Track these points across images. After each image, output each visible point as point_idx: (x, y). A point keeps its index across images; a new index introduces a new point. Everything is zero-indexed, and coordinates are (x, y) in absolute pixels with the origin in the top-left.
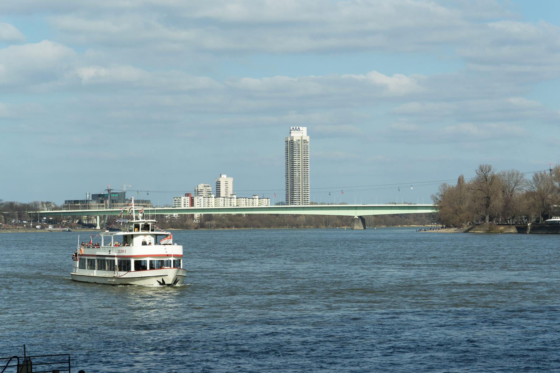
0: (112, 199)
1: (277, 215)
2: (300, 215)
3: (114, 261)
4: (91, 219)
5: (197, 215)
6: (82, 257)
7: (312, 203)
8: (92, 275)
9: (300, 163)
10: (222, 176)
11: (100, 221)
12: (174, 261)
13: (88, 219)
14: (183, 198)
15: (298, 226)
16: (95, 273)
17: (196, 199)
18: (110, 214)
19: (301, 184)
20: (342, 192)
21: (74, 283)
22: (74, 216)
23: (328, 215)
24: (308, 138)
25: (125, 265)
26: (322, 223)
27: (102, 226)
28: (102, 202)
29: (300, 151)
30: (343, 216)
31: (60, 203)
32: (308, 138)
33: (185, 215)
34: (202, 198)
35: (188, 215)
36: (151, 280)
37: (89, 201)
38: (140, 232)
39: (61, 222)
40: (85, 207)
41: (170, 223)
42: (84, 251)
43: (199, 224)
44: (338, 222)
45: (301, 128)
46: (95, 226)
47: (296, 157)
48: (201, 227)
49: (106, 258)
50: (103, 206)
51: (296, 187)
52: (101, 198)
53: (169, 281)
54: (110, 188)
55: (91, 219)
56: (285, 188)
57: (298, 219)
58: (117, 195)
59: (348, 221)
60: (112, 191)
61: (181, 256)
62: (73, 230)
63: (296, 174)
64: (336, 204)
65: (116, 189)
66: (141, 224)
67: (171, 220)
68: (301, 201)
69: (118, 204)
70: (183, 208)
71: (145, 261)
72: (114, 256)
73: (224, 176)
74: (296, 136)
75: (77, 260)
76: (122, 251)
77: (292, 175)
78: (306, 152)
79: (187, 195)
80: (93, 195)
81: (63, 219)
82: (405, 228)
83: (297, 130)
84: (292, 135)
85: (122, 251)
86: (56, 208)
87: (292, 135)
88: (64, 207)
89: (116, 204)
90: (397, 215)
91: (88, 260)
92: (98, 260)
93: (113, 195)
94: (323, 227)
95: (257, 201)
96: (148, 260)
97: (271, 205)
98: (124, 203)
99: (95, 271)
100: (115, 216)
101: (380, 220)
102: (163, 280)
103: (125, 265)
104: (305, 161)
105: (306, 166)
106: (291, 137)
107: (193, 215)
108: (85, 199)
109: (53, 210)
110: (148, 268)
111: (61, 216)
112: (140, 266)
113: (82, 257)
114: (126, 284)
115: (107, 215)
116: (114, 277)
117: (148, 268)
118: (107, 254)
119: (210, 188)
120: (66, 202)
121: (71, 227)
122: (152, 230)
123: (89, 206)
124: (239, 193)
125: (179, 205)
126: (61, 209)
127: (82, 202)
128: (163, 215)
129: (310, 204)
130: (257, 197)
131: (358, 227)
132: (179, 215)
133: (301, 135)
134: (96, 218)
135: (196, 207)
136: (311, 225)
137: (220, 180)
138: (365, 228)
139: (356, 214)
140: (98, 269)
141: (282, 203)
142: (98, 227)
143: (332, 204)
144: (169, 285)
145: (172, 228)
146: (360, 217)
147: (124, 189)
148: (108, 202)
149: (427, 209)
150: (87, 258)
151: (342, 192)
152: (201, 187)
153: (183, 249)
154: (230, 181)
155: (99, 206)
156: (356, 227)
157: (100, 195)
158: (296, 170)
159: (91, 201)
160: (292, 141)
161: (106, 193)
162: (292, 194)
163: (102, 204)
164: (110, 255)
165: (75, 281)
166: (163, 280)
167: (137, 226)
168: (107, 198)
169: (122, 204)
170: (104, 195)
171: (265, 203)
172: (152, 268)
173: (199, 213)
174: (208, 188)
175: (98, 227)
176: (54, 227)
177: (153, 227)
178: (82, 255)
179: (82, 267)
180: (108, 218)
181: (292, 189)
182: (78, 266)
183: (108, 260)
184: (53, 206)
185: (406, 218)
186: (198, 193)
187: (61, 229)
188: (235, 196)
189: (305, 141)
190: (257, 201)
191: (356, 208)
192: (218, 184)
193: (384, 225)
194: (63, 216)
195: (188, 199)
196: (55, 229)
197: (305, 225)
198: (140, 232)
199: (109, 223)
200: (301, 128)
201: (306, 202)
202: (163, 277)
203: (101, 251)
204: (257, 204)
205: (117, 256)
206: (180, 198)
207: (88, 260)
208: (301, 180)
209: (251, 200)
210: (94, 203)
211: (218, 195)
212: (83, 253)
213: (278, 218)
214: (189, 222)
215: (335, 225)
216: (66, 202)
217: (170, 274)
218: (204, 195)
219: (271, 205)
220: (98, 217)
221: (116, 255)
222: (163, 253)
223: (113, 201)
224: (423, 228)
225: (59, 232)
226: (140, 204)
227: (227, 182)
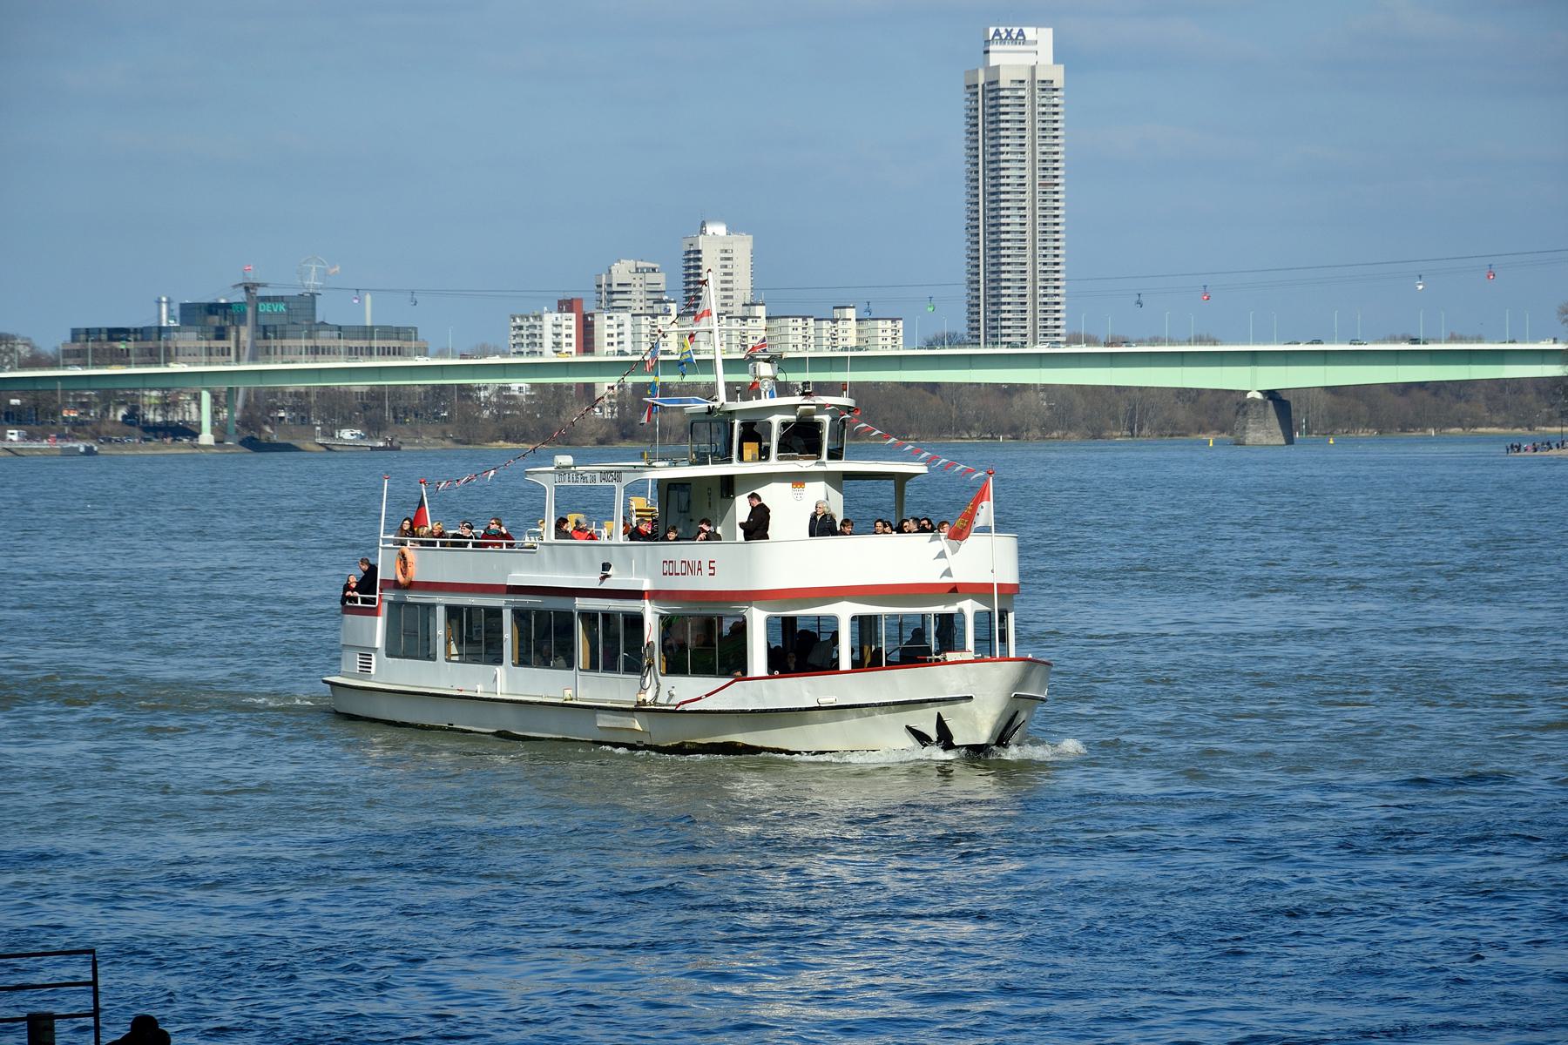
0: (263, 321)
1: (934, 387)
2: (1024, 387)
3: (636, 621)
4: (176, 404)
5: (605, 384)
6: (411, 597)
7: (1073, 339)
8: (480, 691)
9: (1028, 173)
10: (710, 229)
11: (215, 413)
12: (977, 614)
13: (166, 405)
14: (549, 319)
15: (1016, 432)
16: (505, 680)
17: (603, 326)
18: (255, 384)
19: (1028, 260)
20: (1491, 273)
21: (344, 729)
22: (109, 391)
23: (1140, 389)
24: (1057, 75)
25: (707, 640)
26: (1114, 417)
27: (220, 430)
28: (221, 334)
29: (1028, 125)
30: (1200, 392)
31: (53, 339)
32: (1057, 75)
33: (557, 386)
34: (625, 317)
35: (569, 387)
36: (862, 730)
37: (168, 329)
38: (774, 465)
39: (54, 415)
40: (152, 357)
41: (497, 418)
42: (427, 565)
43: (617, 422)
44: (1182, 414)
45: (1030, 33)
46: (191, 431)
47: (1008, 152)
48: (624, 437)
49: (581, 603)
50: (225, 352)
51: (1009, 274)
52: (216, 320)
53: (975, 726)
54: (252, 278)
55: (176, 404)
56: (963, 277)
57: (1017, 402)
58: (282, 307)
59: (1223, 411)
60: (261, 292)
61: (1007, 591)
62: (106, 449)
63: (1011, 220)
64: (1171, 342)
65: (280, 280)
66: (776, 420)
67: (499, 406)
68: (1029, 331)
69: (287, 343)
70: (549, 357)
71: (834, 620)
72: (638, 595)
73: (717, 229)
74: (1009, 62)
75: (374, 612)
76: (692, 568)
77: (995, 227)
78: (1049, 131)
79: (566, 305)
80: (184, 307)
81: (65, 404)
82: (1453, 440)
83: (1015, 41)
84: (994, 60)
85: (692, 568)
86: (36, 361)
87: (994, 60)
88: (67, 354)
89: (273, 343)
90: (1422, 385)
91: (453, 612)
92: (520, 615)
93: (264, 308)
94: (1120, 436)
95: (849, 333)
96: (844, 612)
97: (906, 345)
98: (309, 337)
99: (499, 670)
100: (273, 393)
101: (1349, 408)
102: (941, 725)
103: (707, 640)
104: (1048, 166)
105: (1049, 185)
106: (987, 68)
107: (590, 388)
108: (153, 323)
109: (24, 365)
110: (845, 662)
111: (54, 392)
112: (801, 650)
113: (411, 597)
114: (724, 747)
115: (242, 386)
116: (639, 709)
117: (845, 662)
118: (591, 581)
119: (659, 278)
120: (75, 334)
121: (96, 436)
122: (835, 455)
123: (167, 350)
124: (777, 294)
125: (535, 347)
126: (54, 364)
127: (142, 333)
128: (469, 388)
129: (1068, 343)
130: (851, 313)
131: (1264, 433)
132: (533, 386)
133: (1030, 60)
134: (197, 398)
135: (604, 352)
136: (1070, 428)
137: (702, 243)
138: (1290, 440)
139: (1253, 381)
140: (523, 661)
141: (953, 341)
142: (206, 438)
143: (1155, 341)
144: (976, 753)
145: (507, 439)
146: (1271, 394)
147: (312, 283)
148: (246, 334)
149: (1543, 363)
150: (442, 600)
151: (1491, 273)
152: (622, 271)
153: (1023, 551)
154: (742, 247)
155: (209, 352)
156: (1254, 435)
157: (213, 308)
158: (1009, 199)
159: (176, 329)
160: (993, 86)
161: (239, 296)
162: (995, 301)
163: (221, 344)
164: (607, 585)
165: (350, 715)
166: (941, 725)
167: (753, 432)
168: (240, 319)
169: (304, 343)
170: (228, 306)
171: (886, 339)
172: (867, 660)
173: (613, 380)
174: (651, 277)
175: (206, 438)
176: (30, 437)
177: (839, 428)
178: (411, 586)
179: (410, 640)
180: (247, 400)
181: (995, 281)
182: (379, 642)
183: (589, 617)
184: (24, 351)
185: (1459, 397)
186: (611, 297)
187: (59, 445)
188: (760, 311)
189: (1047, 86)
190: (849, 333)
191: (1254, 358)
192: (693, 259)
193: (1368, 426)
194: (65, 392)
195: (570, 321)
196: (35, 445)
197: (1046, 428)
198: (774, 465)
199: (246, 422)
200: (1030, 33)
201: (1050, 334)
202: (944, 710)
203: (540, 568)
204: (852, 342)
205: (654, 595)
206: (539, 317)
207: (453, 612)
208: (1028, 244)
209: (826, 325)
210: (189, 340)
211: (692, 305)
212: (417, 573)
213: (935, 401)
214: (573, 414)
215: (1172, 430)
216: (75, 334)
217: (975, 690)
218: (637, 307)
219: (906, 345)
220: (206, 397)
221: (646, 585)
222: (931, 574)
223: (264, 332)
224: (1525, 438)
225: (46, 454)
226: (375, 344)
227: (726, 251)
